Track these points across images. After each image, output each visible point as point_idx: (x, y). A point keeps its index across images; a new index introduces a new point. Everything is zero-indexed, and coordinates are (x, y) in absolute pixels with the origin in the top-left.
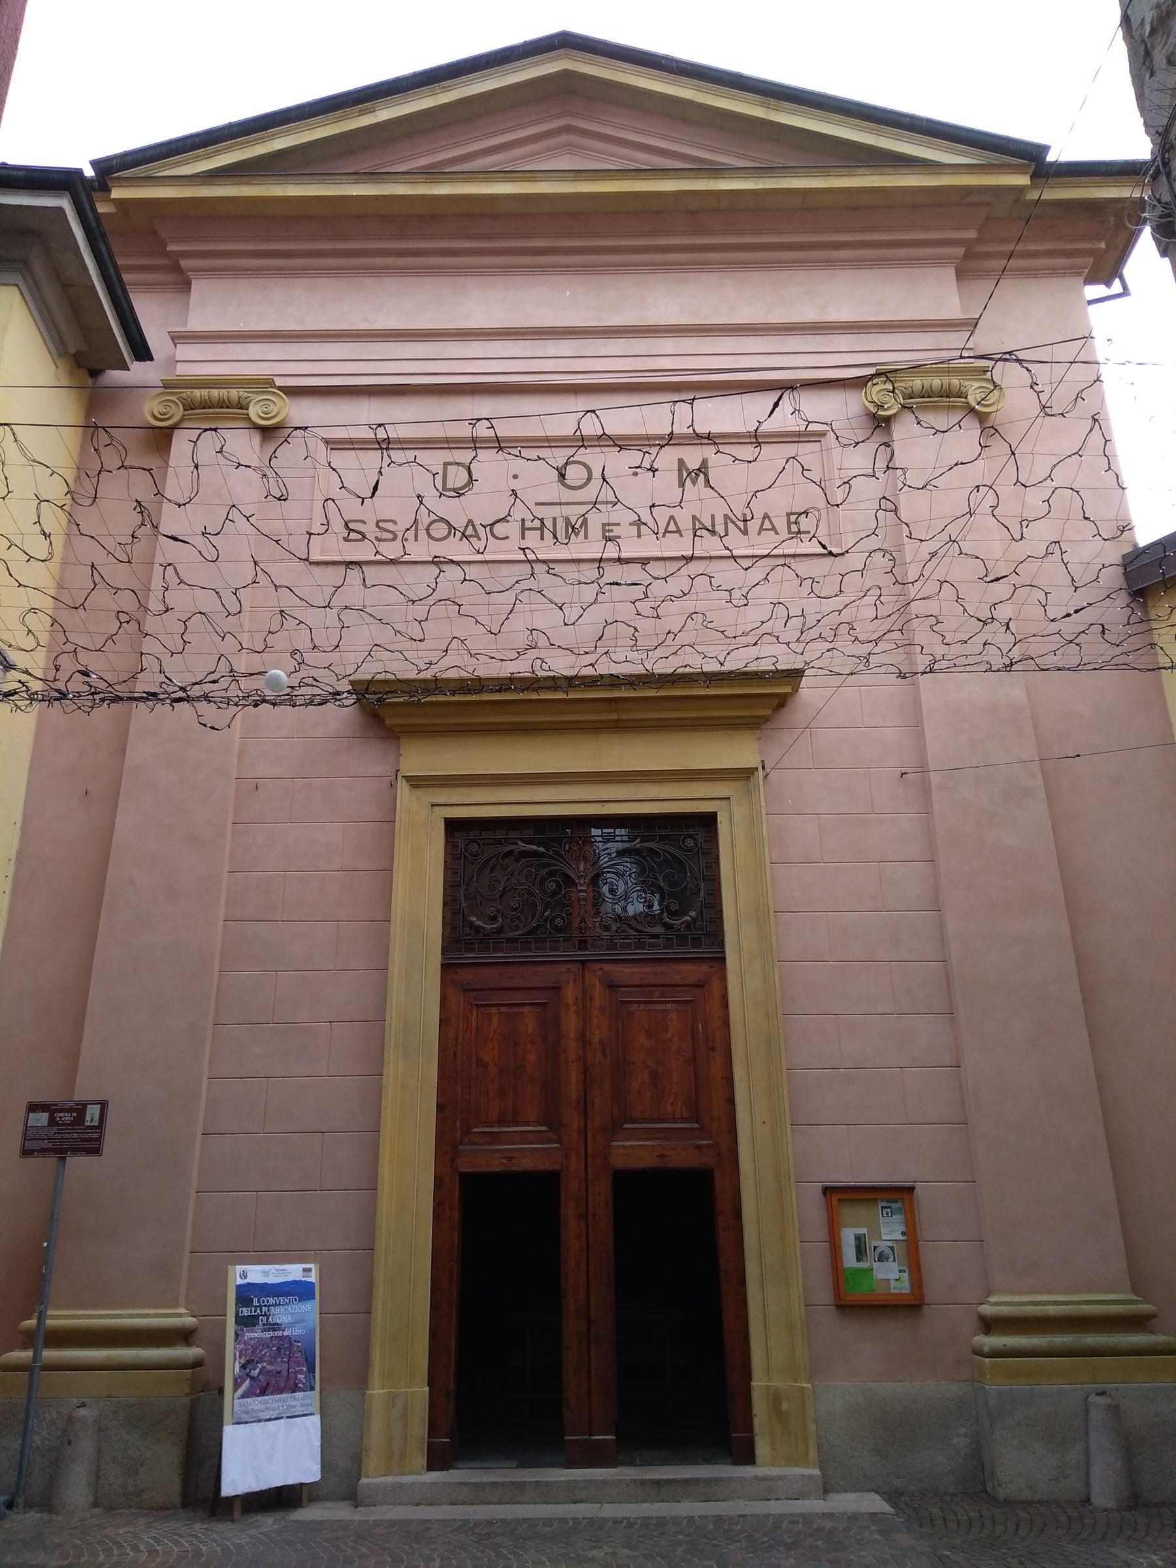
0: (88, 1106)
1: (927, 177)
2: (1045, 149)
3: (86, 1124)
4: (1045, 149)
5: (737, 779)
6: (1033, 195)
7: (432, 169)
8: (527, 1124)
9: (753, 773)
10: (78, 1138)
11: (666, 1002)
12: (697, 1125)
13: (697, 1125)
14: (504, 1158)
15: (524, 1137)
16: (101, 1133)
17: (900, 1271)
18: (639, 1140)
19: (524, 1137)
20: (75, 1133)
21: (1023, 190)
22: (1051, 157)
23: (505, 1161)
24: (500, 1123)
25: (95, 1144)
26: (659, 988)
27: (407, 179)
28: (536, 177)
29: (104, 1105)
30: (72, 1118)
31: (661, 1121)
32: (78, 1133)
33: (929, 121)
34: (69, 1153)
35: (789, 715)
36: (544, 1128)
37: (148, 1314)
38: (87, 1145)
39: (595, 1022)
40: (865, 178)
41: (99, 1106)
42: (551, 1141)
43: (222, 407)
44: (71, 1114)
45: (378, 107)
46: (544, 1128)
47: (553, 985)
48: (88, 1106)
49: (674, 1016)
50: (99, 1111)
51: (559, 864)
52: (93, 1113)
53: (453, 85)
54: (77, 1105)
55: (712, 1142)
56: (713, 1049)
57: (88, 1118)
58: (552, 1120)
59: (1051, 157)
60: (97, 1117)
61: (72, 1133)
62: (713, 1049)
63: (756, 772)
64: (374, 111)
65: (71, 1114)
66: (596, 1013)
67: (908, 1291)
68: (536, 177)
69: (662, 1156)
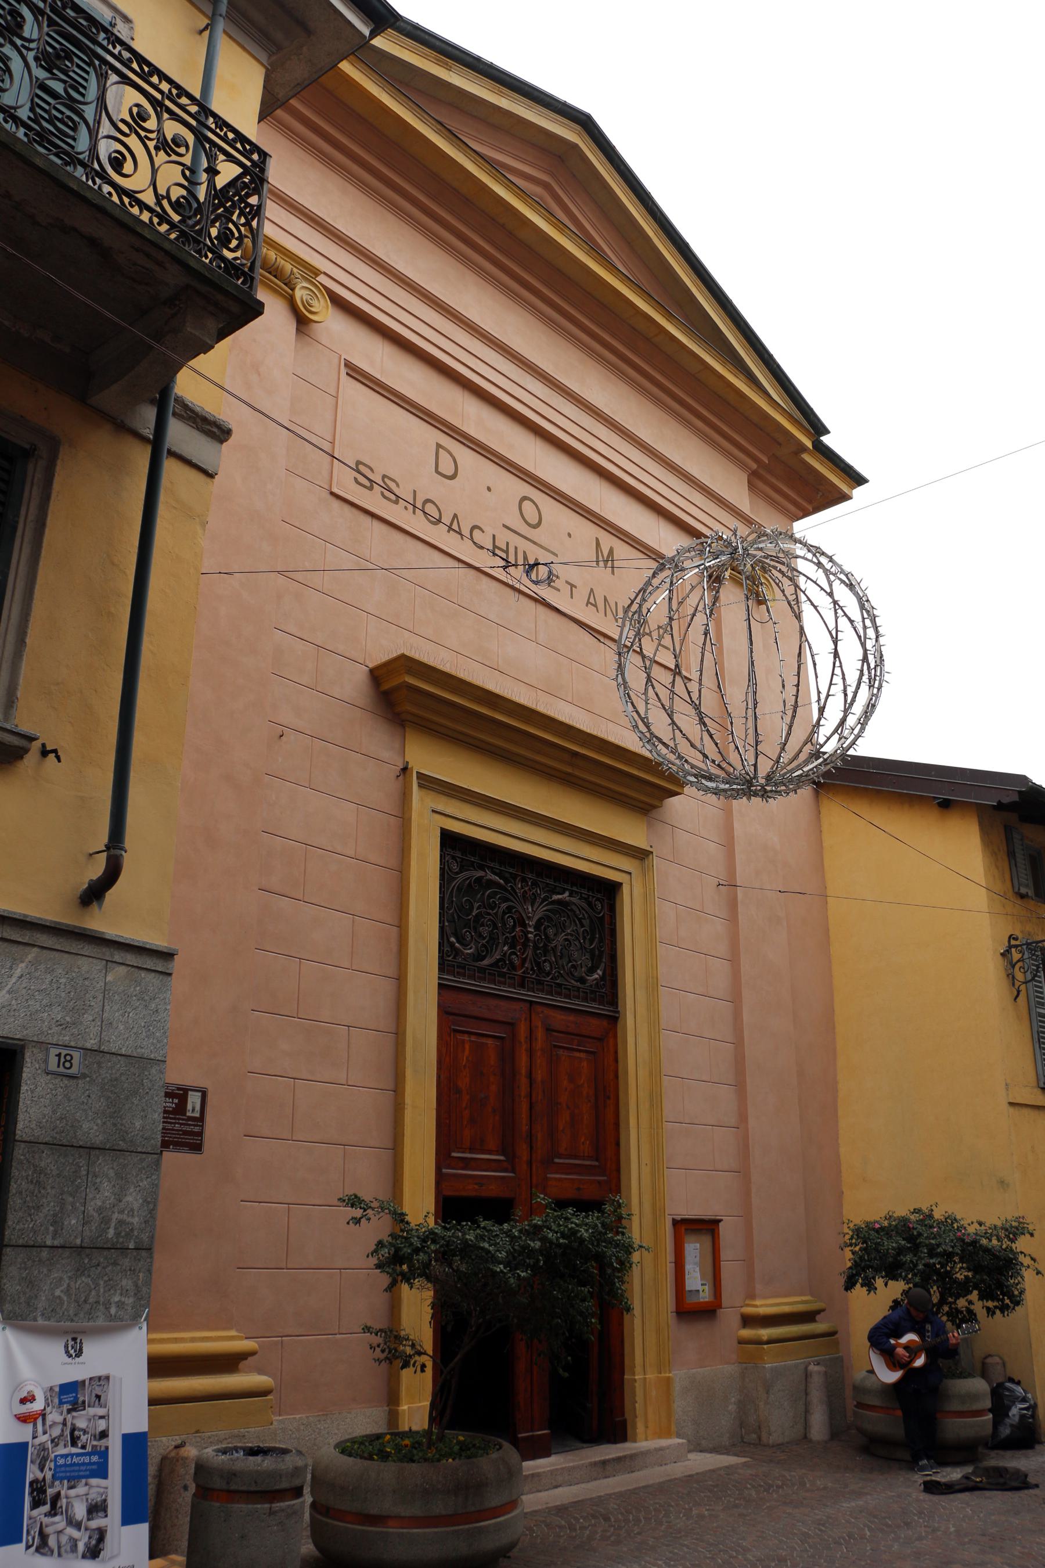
0: (190, 1093)
1: (770, 408)
2: (827, 432)
3: (189, 1114)
4: (827, 432)
5: (634, 857)
6: (806, 457)
7: (496, 165)
8: (489, 1152)
9: (648, 856)
10: (180, 1130)
11: (580, 1051)
12: (597, 1164)
13: (597, 1164)
14: (476, 1184)
15: (488, 1165)
16: (202, 1126)
17: (702, 1285)
18: (562, 1173)
19: (488, 1165)
20: (178, 1123)
21: (806, 450)
22: (825, 439)
23: (476, 1187)
24: (471, 1150)
25: (195, 1140)
26: (577, 1038)
27: (478, 161)
28: (564, 231)
29: (204, 1095)
30: (174, 1105)
31: (576, 1157)
32: (181, 1124)
33: (778, 366)
34: (171, 1147)
35: (654, 813)
36: (502, 1158)
37: (211, 1337)
38: (189, 1139)
39: (539, 1061)
40: (740, 382)
41: (200, 1094)
42: (506, 1171)
43: (270, 273)
44: (173, 1100)
45: (455, 69)
46: (502, 1158)
47: (510, 1021)
48: (190, 1093)
49: (585, 1064)
50: (200, 1100)
51: (515, 901)
52: (194, 1100)
53: (507, 95)
54: (179, 1089)
55: (605, 1178)
56: (609, 1098)
57: (189, 1107)
58: (507, 1148)
59: (825, 439)
60: (198, 1107)
61: (175, 1123)
62: (609, 1098)
63: (651, 856)
64: (450, 70)
65: (173, 1100)
66: (539, 1053)
67: (688, 1302)
68: (564, 231)
69: (579, 1189)
